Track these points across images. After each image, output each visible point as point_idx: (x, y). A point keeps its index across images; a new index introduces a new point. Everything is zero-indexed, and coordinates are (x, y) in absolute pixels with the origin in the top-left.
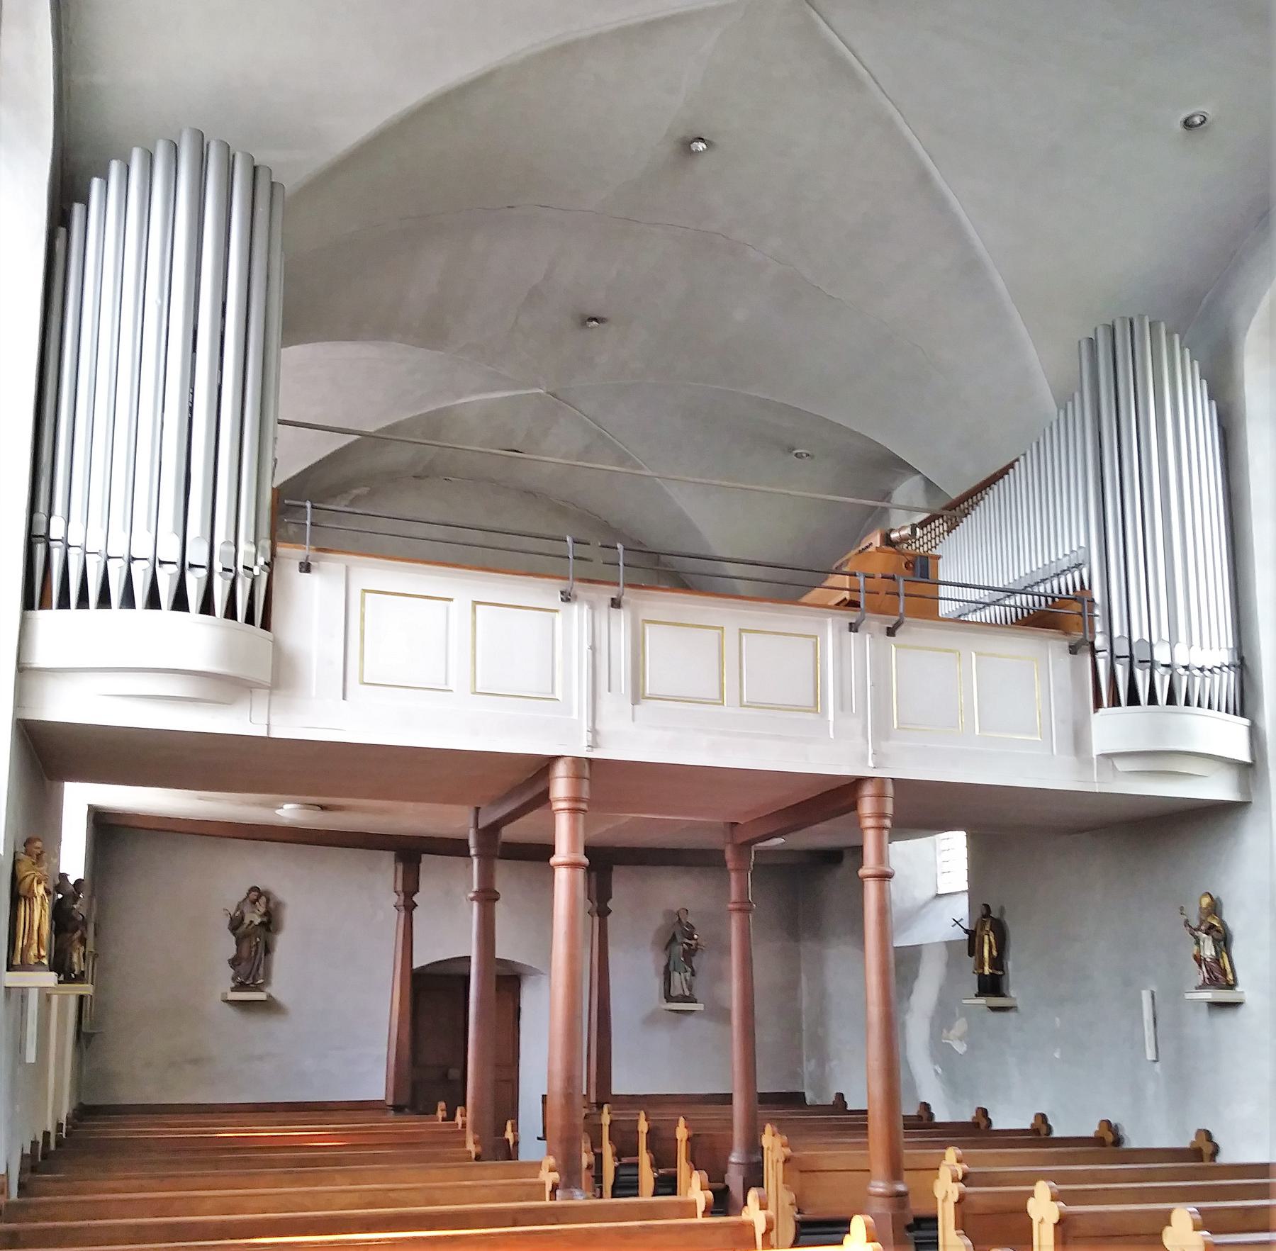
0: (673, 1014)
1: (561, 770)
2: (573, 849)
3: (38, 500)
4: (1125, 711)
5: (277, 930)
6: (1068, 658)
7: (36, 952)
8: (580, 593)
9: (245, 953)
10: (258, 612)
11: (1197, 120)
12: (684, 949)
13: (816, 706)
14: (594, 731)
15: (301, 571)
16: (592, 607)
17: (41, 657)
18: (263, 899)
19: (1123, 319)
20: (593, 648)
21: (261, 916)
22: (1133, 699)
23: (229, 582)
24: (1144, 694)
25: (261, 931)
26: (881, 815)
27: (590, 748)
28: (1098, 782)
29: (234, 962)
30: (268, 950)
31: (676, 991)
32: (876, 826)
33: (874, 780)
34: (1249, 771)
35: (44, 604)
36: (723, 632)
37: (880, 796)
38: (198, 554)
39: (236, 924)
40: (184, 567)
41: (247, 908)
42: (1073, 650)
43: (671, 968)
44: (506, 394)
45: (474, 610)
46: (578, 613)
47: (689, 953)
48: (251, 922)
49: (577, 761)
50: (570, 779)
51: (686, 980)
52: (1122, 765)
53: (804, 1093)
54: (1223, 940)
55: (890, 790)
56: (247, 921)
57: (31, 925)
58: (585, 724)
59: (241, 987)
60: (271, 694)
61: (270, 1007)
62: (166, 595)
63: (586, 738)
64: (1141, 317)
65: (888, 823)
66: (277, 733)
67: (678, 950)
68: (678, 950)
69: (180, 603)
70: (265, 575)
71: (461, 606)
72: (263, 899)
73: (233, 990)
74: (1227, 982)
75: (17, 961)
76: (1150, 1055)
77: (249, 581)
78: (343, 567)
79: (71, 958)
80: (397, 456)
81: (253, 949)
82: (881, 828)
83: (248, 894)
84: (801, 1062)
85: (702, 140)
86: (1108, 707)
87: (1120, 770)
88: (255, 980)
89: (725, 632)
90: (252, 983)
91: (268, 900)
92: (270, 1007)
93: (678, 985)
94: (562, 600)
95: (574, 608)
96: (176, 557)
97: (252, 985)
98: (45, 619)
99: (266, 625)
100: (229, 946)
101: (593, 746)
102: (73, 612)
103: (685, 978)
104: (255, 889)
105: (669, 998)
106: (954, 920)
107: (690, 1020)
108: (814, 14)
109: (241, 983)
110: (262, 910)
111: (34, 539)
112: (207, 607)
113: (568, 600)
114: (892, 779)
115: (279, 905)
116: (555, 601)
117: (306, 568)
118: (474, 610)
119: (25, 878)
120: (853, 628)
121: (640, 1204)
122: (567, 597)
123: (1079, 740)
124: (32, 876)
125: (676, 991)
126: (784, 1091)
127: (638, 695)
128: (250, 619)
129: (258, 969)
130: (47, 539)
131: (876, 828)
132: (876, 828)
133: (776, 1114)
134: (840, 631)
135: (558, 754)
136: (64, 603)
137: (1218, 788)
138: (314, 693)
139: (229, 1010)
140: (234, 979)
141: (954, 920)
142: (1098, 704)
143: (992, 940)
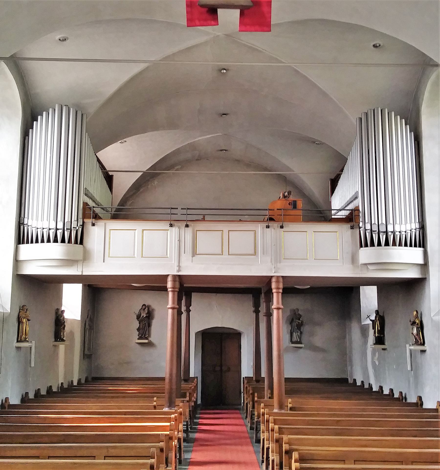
0: (295, 348)
1: (170, 279)
2: (173, 303)
3: (21, 214)
4: (369, 249)
5: (153, 318)
6: (350, 231)
7: (25, 337)
8: (175, 224)
9: (141, 327)
10: (79, 240)
11: (378, 45)
12: (297, 324)
13: (255, 254)
14: (179, 266)
15: (92, 226)
16: (179, 228)
17: (22, 257)
18: (147, 308)
19: (371, 109)
20: (179, 240)
21: (146, 314)
22: (372, 245)
23: (69, 233)
24: (376, 243)
25: (146, 319)
26: (278, 288)
27: (178, 272)
28: (361, 274)
29: (138, 330)
30: (149, 325)
31: (295, 339)
32: (276, 292)
33: (275, 277)
34: (425, 266)
35: (23, 243)
36: (223, 232)
37: (278, 282)
38: (60, 226)
39: (138, 317)
40: (57, 229)
41: (142, 311)
42: (352, 228)
43: (292, 331)
44: (210, 136)
45: (143, 232)
46: (175, 230)
47: (300, 326)
48: (143, 316)
49: (174, 276)
50: (171, 282)
51: (298, 335)
52: (370, 267)
53: (348, 379)
54: (421, 327)
55: (281, 280)
56: (142, 316)
57: (23, 330)
58: (176, 264)
59: (140, 338)
60: (83, 262)
61: (150, 344)
62: (52, 239)
63: (176, 268)
64: (378, 108)
65: (281, 291)
66: (84, 274)
67: (295, 324)
68: (295, 324)
69: (56, 241)
70: (80, 229)
71: (138, 233)
72: (147, 308)
73: (138, 339)
74: (421, 343)
75: (19, 340)
76: (409, 368)
77: (75, 231)
78: (104, 223)
79: (61, 334)
80: (182, 157)
81: (144, 325)
82: (278, 293)
83: (142, 307)
84: (346, 366)
85: (225, 69)
86: (364, 247)
87: (370, 269)
88: (145, 336)
89: (223, 232)
90: (144, 337)
91: (148, 309)
92: (150, 344)
93: (295, 338)
94: (170, 226)
95: (173, 229)
96: (55, 227)
97: (144, 338)
98: (22, 247)
99: (81, 243)
100: (136, 324)
101: (179, 270)
102: (30, 245)
103: (298, 334)
104: (144, 305)
105: (293, 343)
106: (370, 316)
107: (301, 350)
108: (234, 39)
109: (141, 337)
110: (146, 312)
111: (20, 225)
112: (63, 241)
113: (172, 226)
114: (283, 276)
115: (153, 310)
116: (168, 227)
117: (93, 225)
118: (143, 232)
119: (21, 317)
120: (268, 227)
121: (162, 412)
122: (171, 225)
123: (354, 259)
124: (22, 316)
125: (295, 339)
126: (340, 377)
127: (194, 253)
128: (76, 242)
129: (146, 332)
130: (23, 224)
131: (276, 292)
132: (276, 292)
133: (92, 387)
134: (263, 228)
135: (168, 274)
136: (28, 243)
137: (413, 274)
138: (95, 262)
139: (137, 345)
140: (139, 335)
141: (370, 316)
142: (361, 246)
143: (378, 324)
